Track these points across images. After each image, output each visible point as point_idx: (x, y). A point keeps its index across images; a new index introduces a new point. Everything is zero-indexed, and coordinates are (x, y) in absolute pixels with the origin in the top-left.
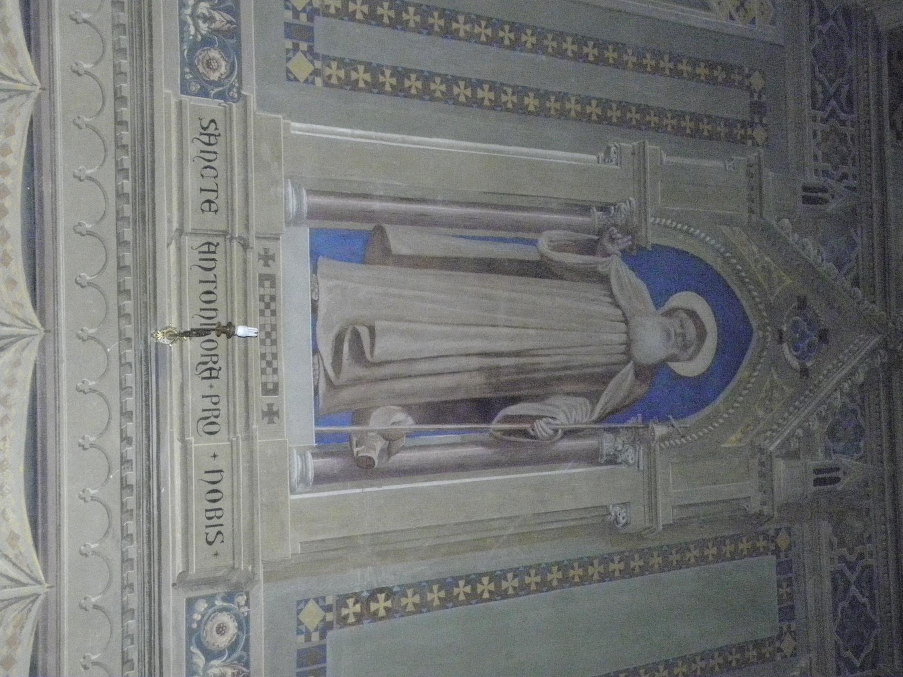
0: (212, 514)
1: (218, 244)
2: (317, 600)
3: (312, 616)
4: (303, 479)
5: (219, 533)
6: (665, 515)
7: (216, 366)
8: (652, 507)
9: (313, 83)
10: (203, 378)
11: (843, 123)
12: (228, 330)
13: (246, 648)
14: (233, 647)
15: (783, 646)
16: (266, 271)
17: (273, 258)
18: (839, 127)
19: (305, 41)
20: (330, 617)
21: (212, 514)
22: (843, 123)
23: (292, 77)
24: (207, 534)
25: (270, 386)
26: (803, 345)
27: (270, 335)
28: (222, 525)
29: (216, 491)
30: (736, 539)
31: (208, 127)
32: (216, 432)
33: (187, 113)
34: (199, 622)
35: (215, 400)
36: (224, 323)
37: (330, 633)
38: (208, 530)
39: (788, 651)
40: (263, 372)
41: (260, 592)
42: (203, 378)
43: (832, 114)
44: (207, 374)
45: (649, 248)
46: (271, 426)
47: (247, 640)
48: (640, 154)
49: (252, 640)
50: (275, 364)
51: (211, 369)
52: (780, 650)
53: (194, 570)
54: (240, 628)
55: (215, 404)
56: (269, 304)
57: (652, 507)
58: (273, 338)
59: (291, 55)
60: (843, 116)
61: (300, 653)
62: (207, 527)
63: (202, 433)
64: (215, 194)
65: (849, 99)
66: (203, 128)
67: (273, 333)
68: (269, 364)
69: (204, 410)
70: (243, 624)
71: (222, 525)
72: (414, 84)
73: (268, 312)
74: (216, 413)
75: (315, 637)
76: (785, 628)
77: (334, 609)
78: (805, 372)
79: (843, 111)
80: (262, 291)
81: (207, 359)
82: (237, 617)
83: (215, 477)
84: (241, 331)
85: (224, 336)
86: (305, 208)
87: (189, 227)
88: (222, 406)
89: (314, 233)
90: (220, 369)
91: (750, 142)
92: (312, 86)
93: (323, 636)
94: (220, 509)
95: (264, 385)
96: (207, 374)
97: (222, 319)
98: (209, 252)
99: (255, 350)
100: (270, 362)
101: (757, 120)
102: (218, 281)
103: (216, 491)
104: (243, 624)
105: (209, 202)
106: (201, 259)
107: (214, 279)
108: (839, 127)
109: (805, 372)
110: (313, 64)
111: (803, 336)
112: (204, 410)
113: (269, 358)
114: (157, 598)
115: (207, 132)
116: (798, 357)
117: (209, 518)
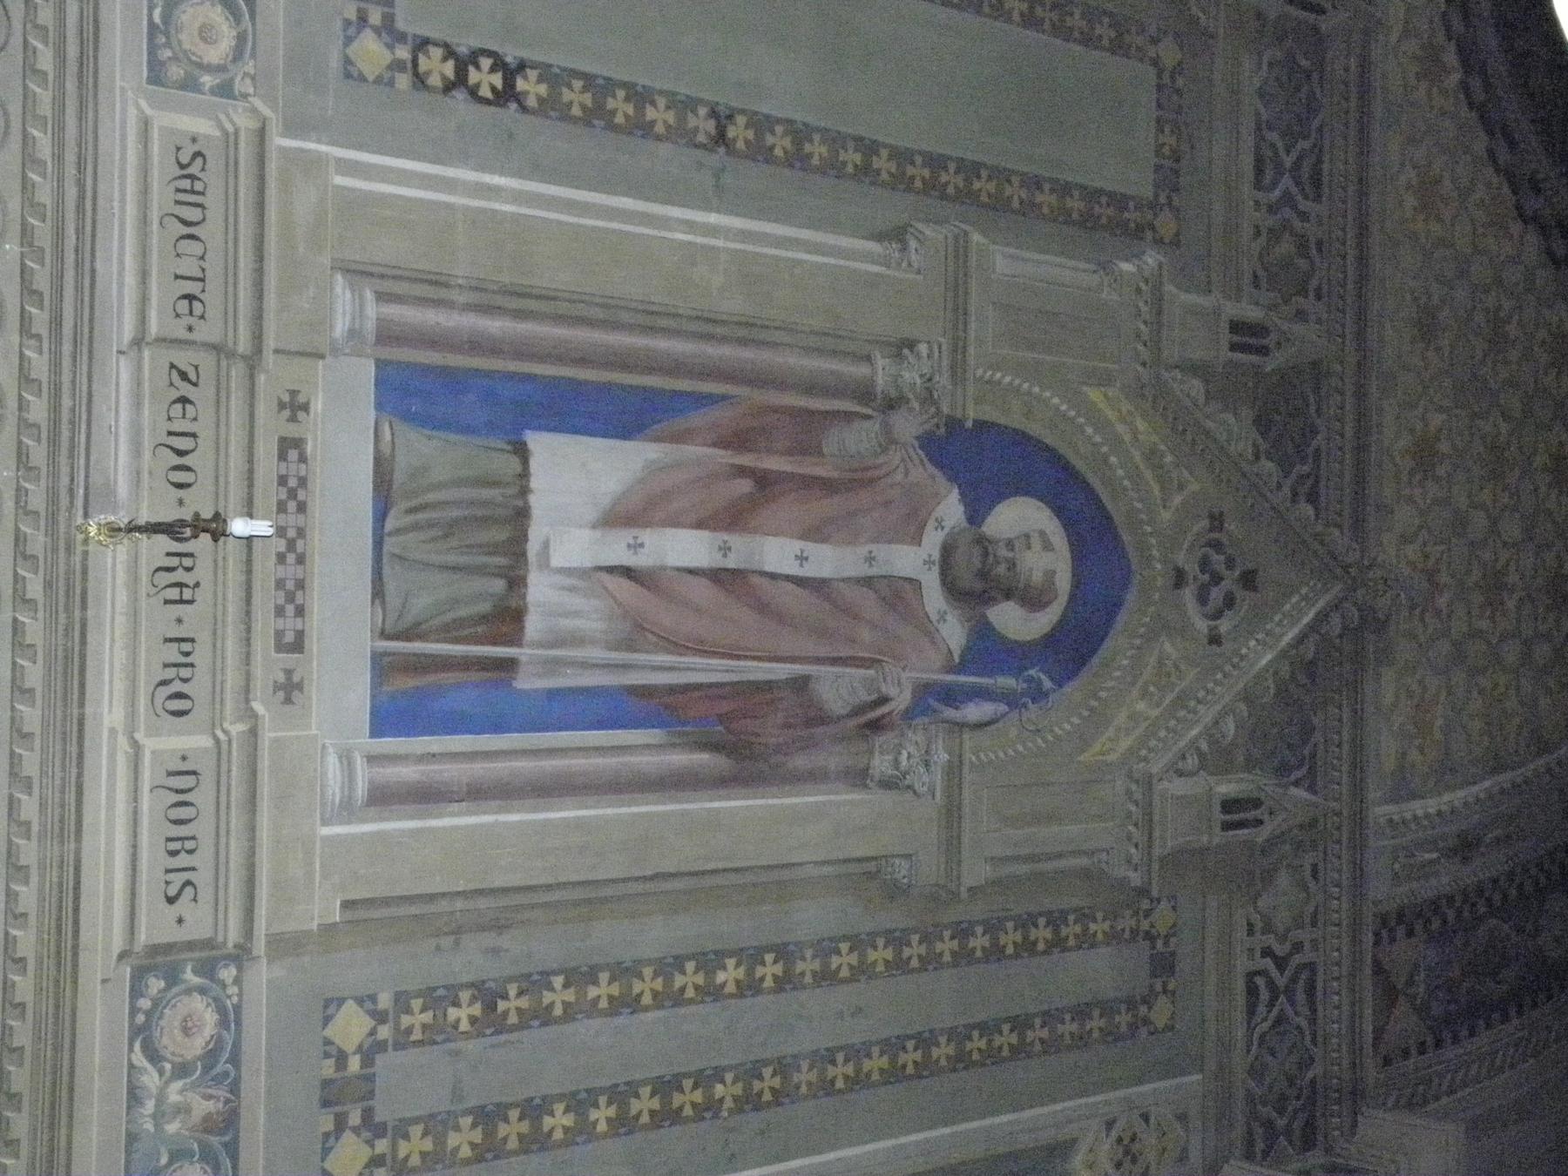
0: (173, 846)
1: (197, 585)
2: (360, 1001)
3: (351, 1027)
4: (353, 333)
5: (188, 883)
6: (975, 872)
7: (188, 578)
8: (952, 845)
9: (391, 83)
10: (167, 602)
11: (1304, 216)
12: (215, 528)
13: (235, 1060)
14: (211, 1056)
15: (1153, 1016)
16: (292, 431)
17: (299, 686)
18: (1297, 224)
19: (378, 3)
20: (384, 1032)
21: (173, 846)
22: (1304, 216)
23: (330, 1011)
24: (167, 883)
25: (289, 637)
26: (1216, 595)
27: (293, 546)
28: (194, 869)
29: (186, 804)
30: (1085, 916)
31: (189, 165)
32: (189, 485)
33: (155, 134)
34: (148, 1014)
35: (186, 647)
36: (207, 514)
37: (400, 25)
38: (171, 876)
39: (1160, 1023)
40: (280, 611)
41: (262, 974)
42: (167, 602)
43: (1287, 199)
44: (173, 593)
45: (969, 424)
46: (287, 708)
47: (237, 1046)
48: (960, 250)
49: (246, 1047)
50: (301, 495)
51: (180, 585)
52: (1146, 1021)
53: (142, 938)
54: (223, 1023)
55: (187, 654)
56: (293, 497)
57: (952, 845)
58: (299, 550)
59: (352, 31)
60: (1304, 205)
61: (326, 1083)
62: (168, 871)
63: (160, 711)
64: (200, 284)
65: (1317, 182)
66: (182, 167)
67: (299, 594)
68: (292, 494)
69: (166, 666)
70: (230, 1018)
71: (194, 869)
72: (576, 97)
73: (291, 558)
74: (185, 673)
75: (354, 1064)
76: (1159, 988)
77: (391, 1017)
78: (1215, 640)
79: (1306, 198)
80: (281, 572)
81: (174, 561)
82: (221, 1010)
83: (188, 782)
84: (239, 526)
85: (205, 538)
86: (370, 326)
87: (154, 328)
88: (201, 657)
89: (381, 365)
90: (197, 585)
91: (1149, 235)
92: (387, 89)
93: (367, 1061)
94: (193, 838)
95: (279, 634)
96: (173, 593)
97: (200, 503)
98: (193, 192)
99: (266, 569)
100: (293, 597)
101: (1162, 200)
102: (209, 274)
103: (186, 804)
104: (230, 1018)
105: (190, 298)
106: (177, 202)
107: (200, 275)
108: (1297, 224)
109: (1215, 640)
110: (372, 1146)
111: (1217, 579)
112: (166, 666)
113: (292, 483)
114: (86, 336)
115: (190, 171)
116: (1206, 616)
117: (173, 853)
